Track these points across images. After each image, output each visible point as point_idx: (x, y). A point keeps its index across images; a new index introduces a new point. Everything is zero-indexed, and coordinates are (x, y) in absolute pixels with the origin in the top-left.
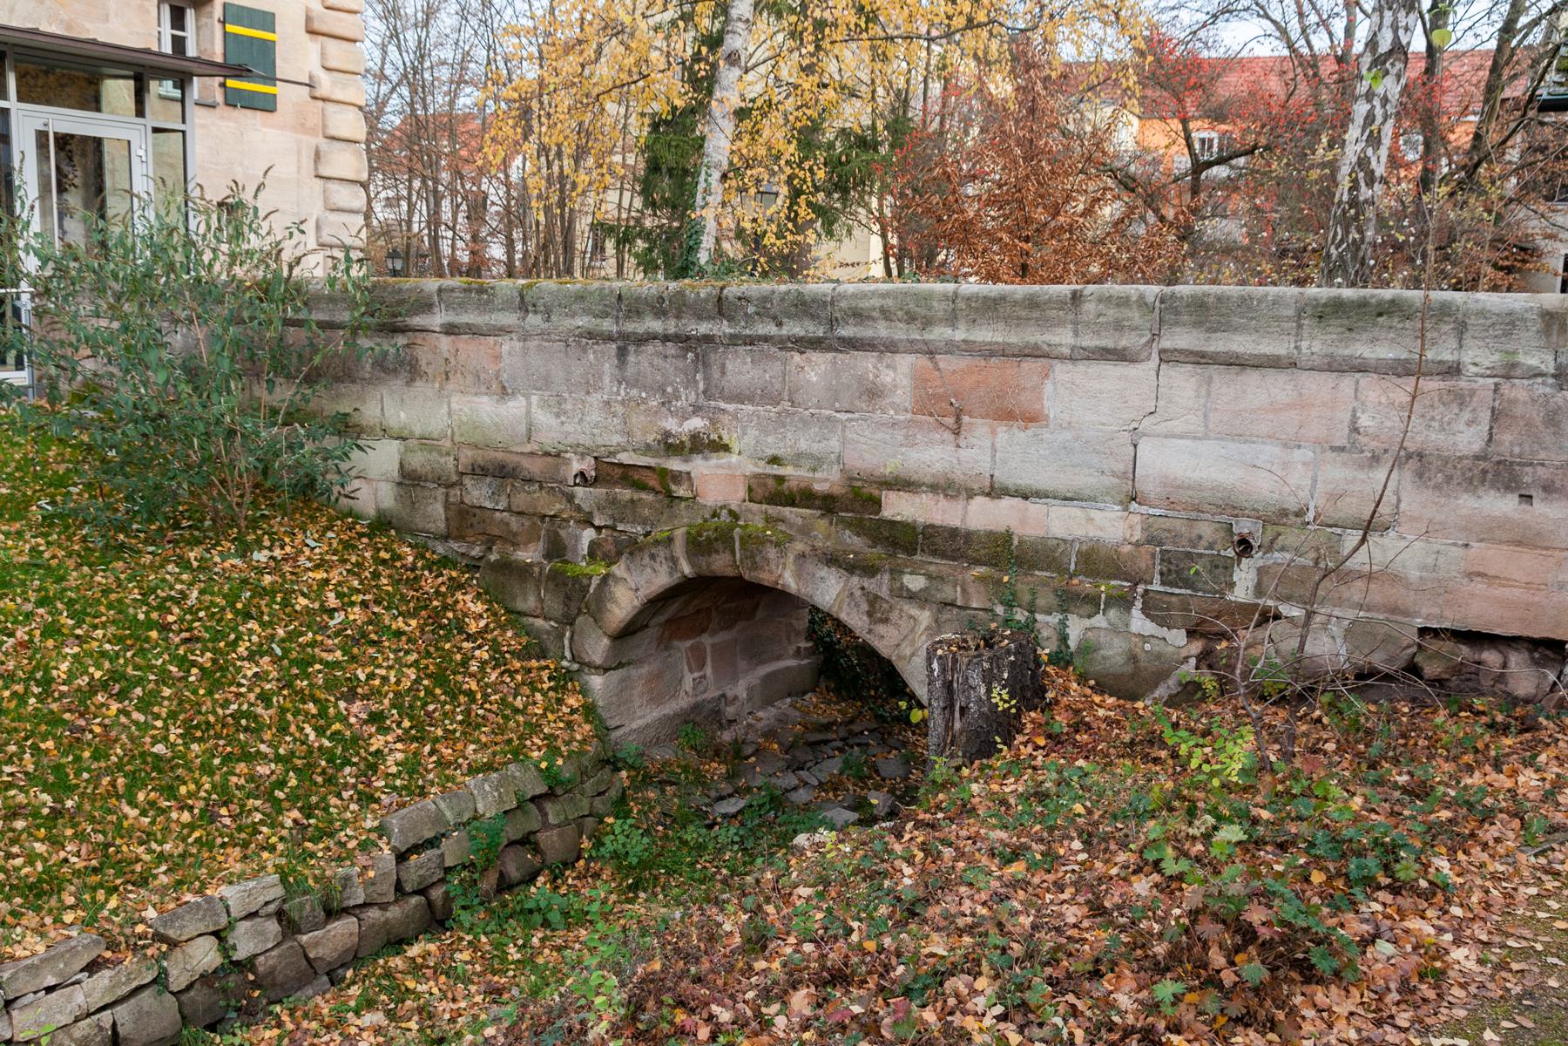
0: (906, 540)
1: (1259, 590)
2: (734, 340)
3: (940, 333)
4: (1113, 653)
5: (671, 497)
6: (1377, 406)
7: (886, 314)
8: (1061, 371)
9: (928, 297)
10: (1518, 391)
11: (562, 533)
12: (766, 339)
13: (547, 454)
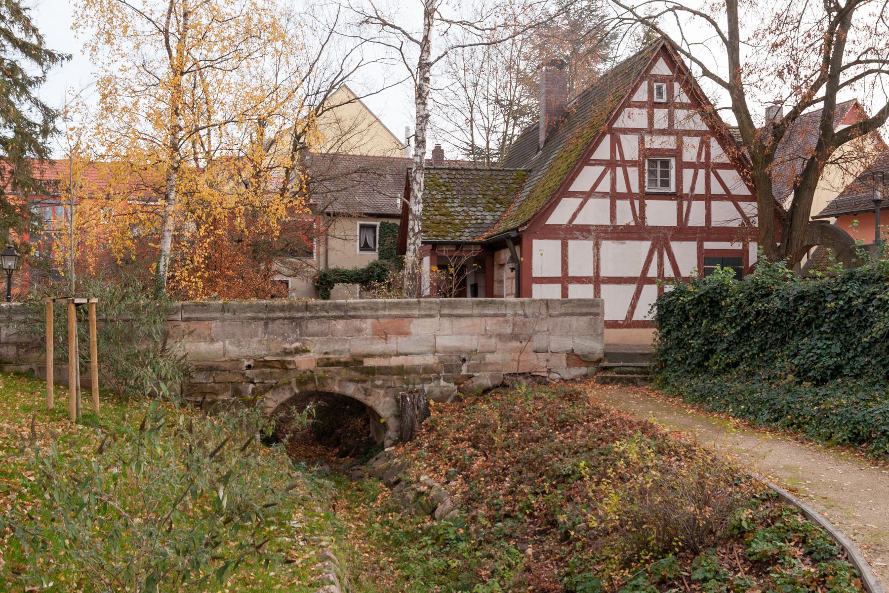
0: (372, 372)
1: (468, 371)
2: (312, 318)
3: (381, 313)
4: (437, 392)
5: (287, 369)
6: (491, 324)
7: (364, 308)
8: (415, 321)
9: (377, 303)
10: (517, 319)
11: (240, 387)
12: (324, 317)
13: (233, 360)
